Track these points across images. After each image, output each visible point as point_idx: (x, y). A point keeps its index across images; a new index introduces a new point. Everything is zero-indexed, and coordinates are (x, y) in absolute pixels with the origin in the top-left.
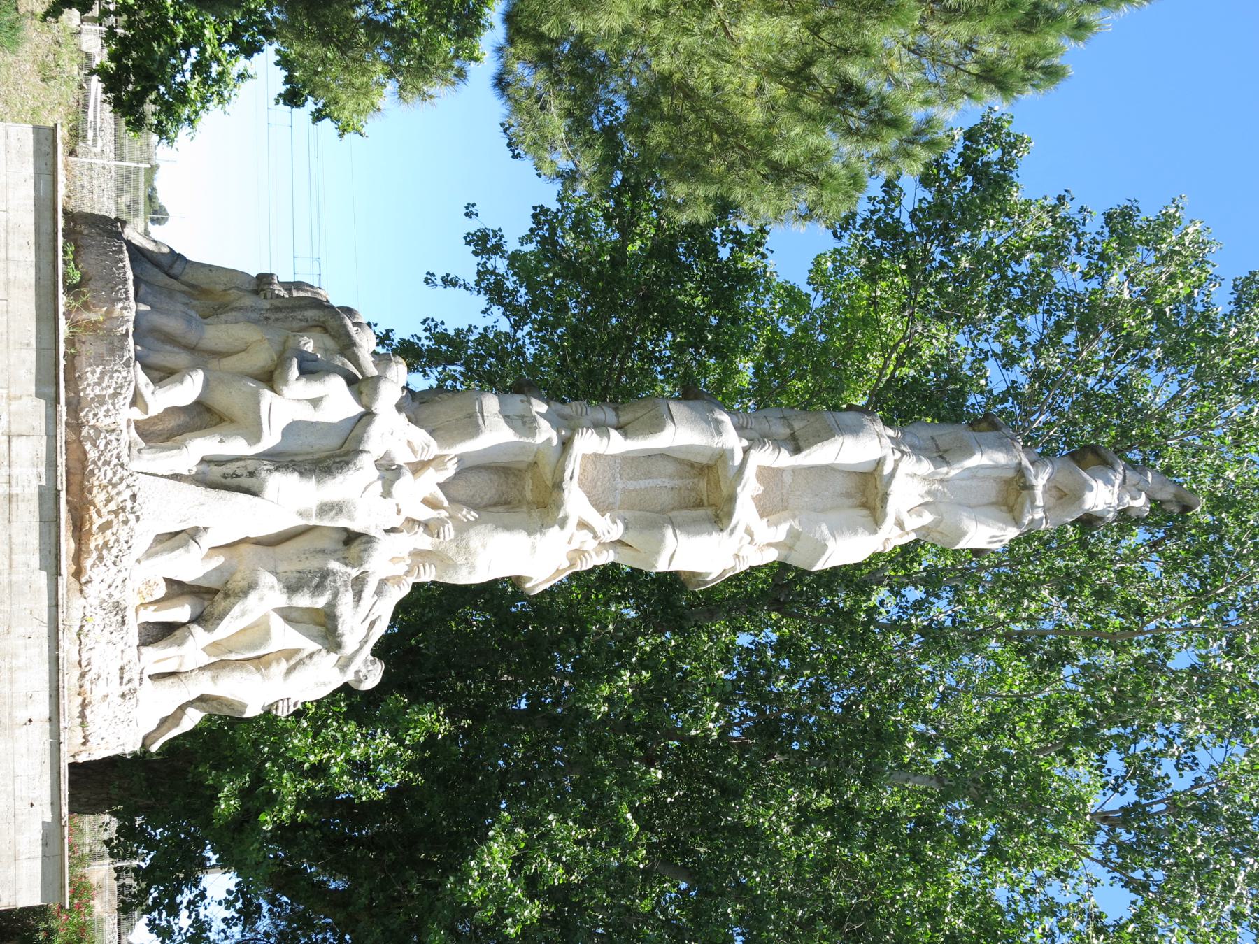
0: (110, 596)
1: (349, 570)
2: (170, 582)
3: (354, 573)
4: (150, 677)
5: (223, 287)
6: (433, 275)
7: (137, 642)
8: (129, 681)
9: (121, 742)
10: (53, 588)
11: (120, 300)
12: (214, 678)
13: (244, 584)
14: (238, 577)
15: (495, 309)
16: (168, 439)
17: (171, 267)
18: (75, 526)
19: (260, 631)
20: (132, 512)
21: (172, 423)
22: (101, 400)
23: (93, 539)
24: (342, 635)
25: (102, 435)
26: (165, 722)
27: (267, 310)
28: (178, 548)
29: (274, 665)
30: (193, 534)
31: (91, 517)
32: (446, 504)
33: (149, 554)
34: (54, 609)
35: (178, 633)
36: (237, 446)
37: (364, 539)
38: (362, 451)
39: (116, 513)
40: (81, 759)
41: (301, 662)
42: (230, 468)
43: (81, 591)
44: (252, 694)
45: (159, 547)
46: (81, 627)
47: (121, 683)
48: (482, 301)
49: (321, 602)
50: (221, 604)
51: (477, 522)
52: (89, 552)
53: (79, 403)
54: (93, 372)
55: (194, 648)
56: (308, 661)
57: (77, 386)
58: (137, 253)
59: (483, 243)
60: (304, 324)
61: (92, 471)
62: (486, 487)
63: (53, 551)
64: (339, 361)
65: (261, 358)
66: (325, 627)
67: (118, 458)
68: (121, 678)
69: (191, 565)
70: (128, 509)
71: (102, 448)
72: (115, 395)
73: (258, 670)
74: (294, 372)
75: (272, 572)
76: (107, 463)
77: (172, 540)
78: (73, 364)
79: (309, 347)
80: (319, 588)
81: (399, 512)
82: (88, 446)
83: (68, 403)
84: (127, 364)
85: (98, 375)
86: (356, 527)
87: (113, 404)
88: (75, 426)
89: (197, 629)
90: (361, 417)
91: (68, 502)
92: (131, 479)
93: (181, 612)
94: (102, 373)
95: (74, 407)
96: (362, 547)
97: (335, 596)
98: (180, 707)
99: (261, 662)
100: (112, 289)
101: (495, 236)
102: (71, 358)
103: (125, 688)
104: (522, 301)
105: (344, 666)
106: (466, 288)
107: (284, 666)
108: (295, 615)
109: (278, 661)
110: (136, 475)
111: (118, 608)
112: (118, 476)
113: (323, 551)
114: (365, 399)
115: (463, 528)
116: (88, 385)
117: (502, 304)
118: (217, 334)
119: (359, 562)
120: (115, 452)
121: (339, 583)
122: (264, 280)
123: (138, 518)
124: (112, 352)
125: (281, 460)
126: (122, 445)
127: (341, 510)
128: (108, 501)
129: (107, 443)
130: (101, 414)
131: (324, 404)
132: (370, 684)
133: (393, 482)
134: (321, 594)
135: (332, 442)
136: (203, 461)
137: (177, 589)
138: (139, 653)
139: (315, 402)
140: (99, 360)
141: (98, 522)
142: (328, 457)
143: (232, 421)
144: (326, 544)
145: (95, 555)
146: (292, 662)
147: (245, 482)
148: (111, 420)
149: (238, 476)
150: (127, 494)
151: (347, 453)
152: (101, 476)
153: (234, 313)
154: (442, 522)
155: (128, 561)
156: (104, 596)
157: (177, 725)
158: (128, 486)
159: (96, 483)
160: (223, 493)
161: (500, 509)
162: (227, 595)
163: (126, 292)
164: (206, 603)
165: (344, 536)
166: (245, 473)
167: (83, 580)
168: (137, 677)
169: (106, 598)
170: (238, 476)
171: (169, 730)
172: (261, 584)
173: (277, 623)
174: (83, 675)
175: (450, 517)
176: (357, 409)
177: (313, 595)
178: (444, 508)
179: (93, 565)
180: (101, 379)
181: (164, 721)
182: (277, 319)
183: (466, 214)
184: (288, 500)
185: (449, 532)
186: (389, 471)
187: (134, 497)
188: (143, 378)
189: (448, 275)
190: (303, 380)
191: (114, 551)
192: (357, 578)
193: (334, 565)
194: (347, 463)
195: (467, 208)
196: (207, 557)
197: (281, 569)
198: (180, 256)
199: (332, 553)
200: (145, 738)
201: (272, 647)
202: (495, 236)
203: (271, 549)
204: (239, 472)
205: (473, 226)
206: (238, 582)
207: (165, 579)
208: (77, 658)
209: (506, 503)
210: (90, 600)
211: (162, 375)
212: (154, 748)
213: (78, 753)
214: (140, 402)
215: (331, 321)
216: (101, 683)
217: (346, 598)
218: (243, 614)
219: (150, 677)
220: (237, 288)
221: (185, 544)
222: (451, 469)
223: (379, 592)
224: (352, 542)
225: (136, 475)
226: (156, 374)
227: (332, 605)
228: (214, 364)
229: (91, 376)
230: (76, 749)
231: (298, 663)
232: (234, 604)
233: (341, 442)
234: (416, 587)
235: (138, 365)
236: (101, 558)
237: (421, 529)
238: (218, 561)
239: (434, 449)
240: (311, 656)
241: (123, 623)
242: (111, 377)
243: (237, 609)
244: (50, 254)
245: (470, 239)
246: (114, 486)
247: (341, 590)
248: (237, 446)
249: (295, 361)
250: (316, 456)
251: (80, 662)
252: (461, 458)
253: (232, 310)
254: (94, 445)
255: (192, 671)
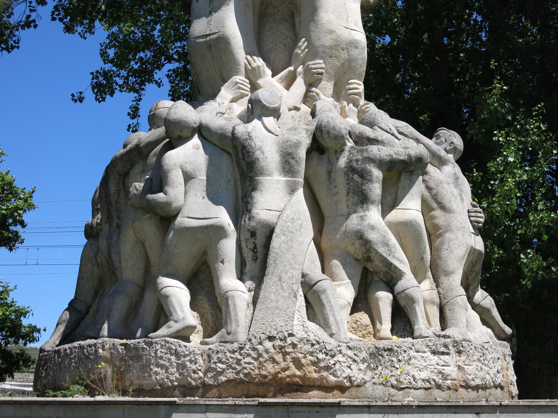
0: (364, 361)
1: (347, 149)
2: (355, 309)
3: (350, 144)
4: (443, 329)
5: (96, 267)
6: (129, 126)
7: (410, 339)
8: (446, 346)
9: (502, 357)
10: (357, 409)
11: (96, 351)
12: (448, 274)
13: (357, 243)
14: (351, 249)
15: (156, 77)
16: (220, 310)
17: (79, 312)
18: (297, 391)
19: (404, 230)
20: (284, 339)
21: (206, 305)
22: (181, 367)
23: (309, 375)
24: (409, 156)
25: (213, 366)
26: (486, 320)
27: (110, 226)
28: (320, 300)
29: (436, 221)
30: (308, 286)
31: (288, 376)
32: (291, 68)
33: (325, 325)
34: (372, 410)
35: (402, 303)
36: (229, 247)
37: (319, 134)
38: (233, 133)
39: (285, 354)
40: (515, 390)
41: (435, 197)
42: (248, 254)
43: (358, 386)
44: (463, 240)
45: (320, 317)
46: (393, 386)
47: (448, 354)
48: (150, 87)
49: (377, 173)
50: (377, 264)
51: (308, 40)
52: (322, 378)
53: (184, 386)
54: (157, 373)
55: (421, 290)
56: (434, 191)
57: (168, 388)
58: (66, 338)
59: (103, 87)
60: (122, 194)
61: (246, 375)
62: (277, 33)
63: (317, 409)
64: (152, 159)
65: (148, 228)
66: (402, 173)
67: (234, 352)
68: (443, 353)
69: (341, 291)
70: (281, 343)
71: (224, 366)
72: (177, 355)
73: (441, 235)
74: (160, 196)
75: (348, 218)
76: (238, 362)
77: (315, 308)
78: (149, 391)
79: (139, 185)
80: (364, 176)
81: (297, 109)
82: (223, 379)
83: (184, 396)
84: (150, 344)
85: (159, 370)
86: (306, 141)
87: (185, 356)
88: (205, 389)
89: (401, 285)
90: (202, 137)
91: (274, 396)
92: (254, 340)
93: (384, 299)
94: (158, 365)
95: (187, 389)
96: (325, 136)
97: (371, 160)
98: (473, 308)
99: (435, 233)
100: (87, 358)
101: (97, 77)
102: (139, 392)
103: (452, 350)
104: (149, 54)
105: (440, 162)
106: (140, 100)
107: (438, 213)
108: (389, 200)
109: (433, 218)
110: (250, 336)
111: (376, 355)
112: (251, 352)
113: (329, 173)
114: (185, 133)
115: (314, 52)
116: (168, 378)
117: (152, 71)
118: (130, 269)
119: (339, 139)
120: (228, 354)
121: (359, 157)
122: (90, 232)
123: (291, 335)
124: (139, 358)
125: (241, 208)
126: (222, 348)
127: (289, 154)
128: (273, 361)
129: (220, 361)
130: (194, 367)
131: (189, 168)
132: (458, 141)
133: (264, 106)
134: (369, 173)
135: (225, 162)
136: (241, 277)
137: (362, 303)
138: (421, 337)
139: (188, 177)
140: (146, 367)
141: (293, 370)
142: (239, 165)
143: (205, 253)
144: (322, 170)
145: (325, 374)
146: (435, 205)
147: (260, 240)
148: (200, 361)
149: (255, 247)
150: (268, 344)
151: (235, 147)
152: (249, 365)
153: (113, 255)
154: (308, 72)
155: (331, 344)
156: (363, 366)
157: (488, 311)
158: (260, 343)
159: (257, 371)
160: (270, 260)
161: (297, 20)
162: (369, 259)
163: (90, 346)
164: (376, 278)
165: (315, 154)
166: (252, 240)
167: (348, 384)
168: (443, 340)
169: (366, 364)
170: (255, 247)
171: (493, 318)
172: (359, 227)
173: (395, 215)
174: (439, 387)
175: (303, 64)
176: (196, 140)
177: (371, 181)
178: (296, 69)
179: (335, 375)
180: (162, 367)
181: (485, 322)
182: (119, 217)
183: (81, 101)
184: (279, 201)
185: (318, 64)
186: (257, 110)
187: (271, 338)
188: (163, 331)
189: (129, 114)
190: (167, 188)
191: (321, 356)
192: (356, 143)
193: (342, 161)
194: (244, 147)
195: (76, 101)
196: (333, 277)
197: (345, 211)
198: (71, 304)
199: (332, 163)
200: (499, 338)
201: (419, 218)
202: (97, 77)
203: (327, 220)
204: (251, 246)
205: (90, 95)
206: (355, 248)
207: (352, 313)
208: (422, 392)
209: (292, 16)
210: (367, 378)
211: (162, 313)
212: (508, 330)
213: (510, 393)
214: (184, 333)
215: (120, 170)
216: (447, 370)
217: (374, 150)
218: (386, 244)
219: (443, 329)
220: (96, 255)
221: (318, 295)
222: (259, 62)
223: (371, 124)
224: (322, 144)
225: (250, 336)
226: (162, 320)
227: (381, 164)
228: (154, 270)
229: (159, 375)
230: (507, 395)
231: (436, 200)
232: (377, 252)
233: (225, 155)
234: (368, 97)
235: (151, 335)
236: (327, 368)
237: (314, 89)
238: (336, 265)
239: (240, 78)
240: (429, 188)
241: (390, 350)
242: (161, 358)
243: (382, 250)
244: (34, 408)
245: (100, 99)
246: (260, 355)
247: (365, 155)
248: (229, 247)
249: (150, 196)
250: (238, 177)
251: (426, 389)
252: (248, 52)
253: (110, 256)
254: (221, 373)
255: (439, 293)
